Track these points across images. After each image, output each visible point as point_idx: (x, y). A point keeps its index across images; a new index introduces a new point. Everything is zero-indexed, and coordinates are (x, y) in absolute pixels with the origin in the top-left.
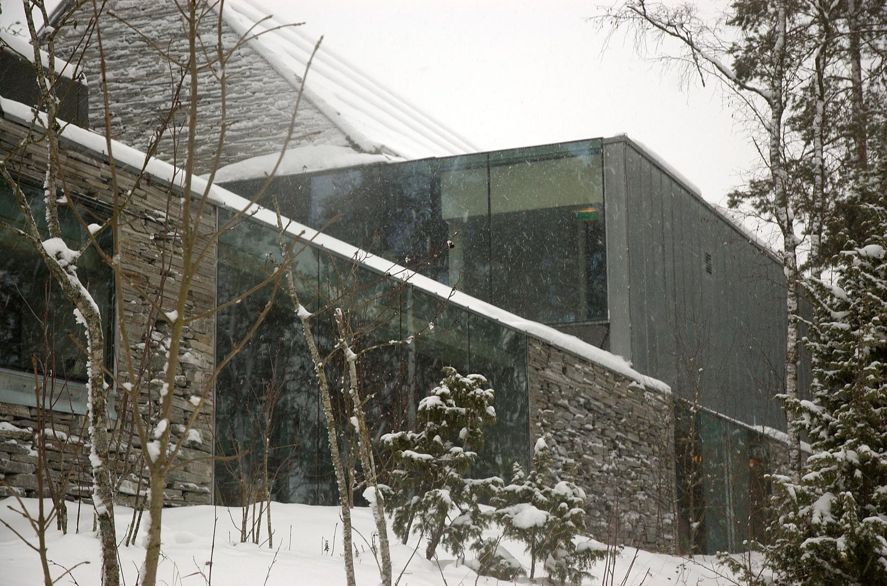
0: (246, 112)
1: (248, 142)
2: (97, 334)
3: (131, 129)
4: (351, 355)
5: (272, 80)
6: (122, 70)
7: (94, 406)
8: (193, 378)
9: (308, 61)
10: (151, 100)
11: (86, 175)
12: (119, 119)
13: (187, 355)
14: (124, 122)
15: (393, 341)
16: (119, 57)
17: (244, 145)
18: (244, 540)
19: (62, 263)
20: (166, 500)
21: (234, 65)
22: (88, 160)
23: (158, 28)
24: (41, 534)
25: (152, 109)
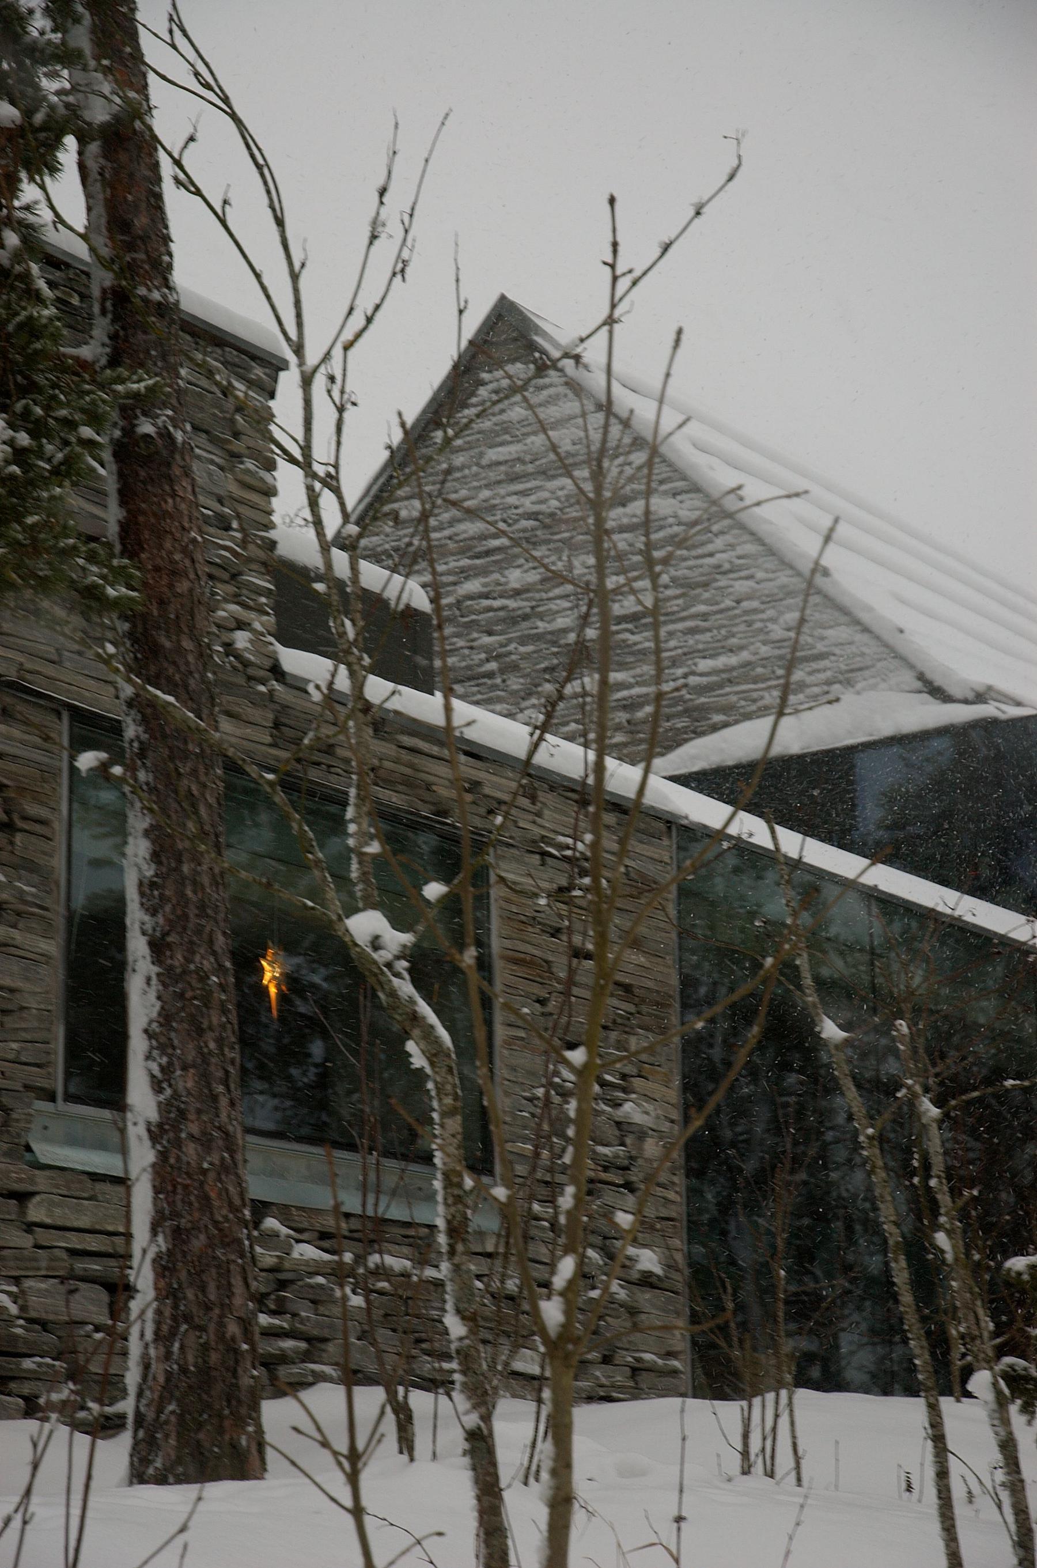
0: (726, 638)
1: (730, 694)
2: (449, 1087)
3: (515, 683)
4: (931, 1111)
5: (771, 576)
6: (496, 576)
7: (449, 1222)
8: (641, 1149)
9: (831, 546)
10: (550, 627)
11: (432, 779)
12: (493, 666)
13: (628, 1107)
14: (502, 671)
15: (1011, 1082)
16: (488, 553)
17: (723, 701)
18: (746, 1471)
19: (382, 957)
20: (602, 1386)
21: (700, 551)
22: (435, 750)
23: (560, 493)
24: (353, 1479)
25: (554, 643)
